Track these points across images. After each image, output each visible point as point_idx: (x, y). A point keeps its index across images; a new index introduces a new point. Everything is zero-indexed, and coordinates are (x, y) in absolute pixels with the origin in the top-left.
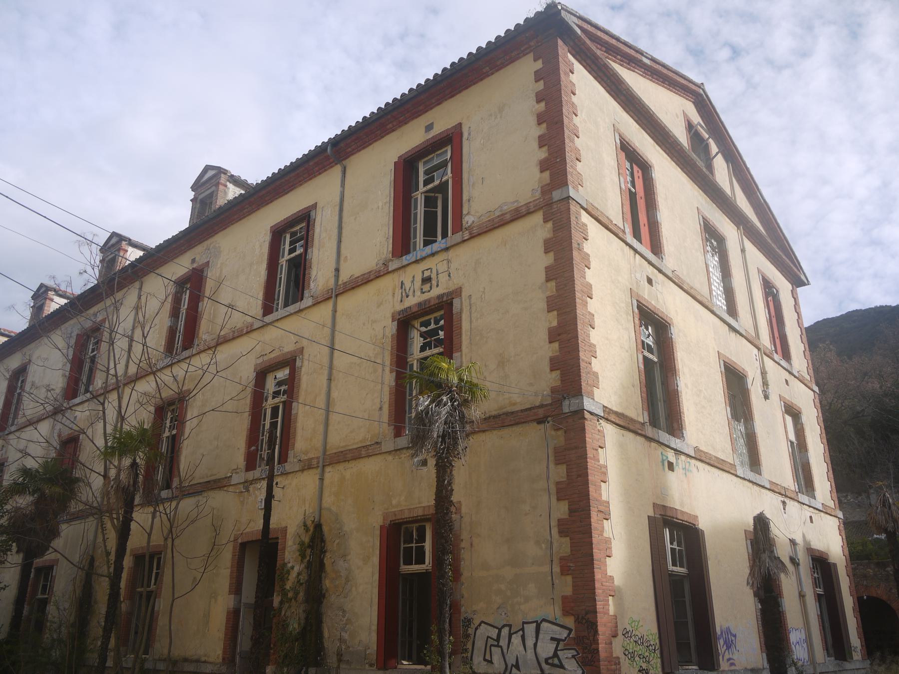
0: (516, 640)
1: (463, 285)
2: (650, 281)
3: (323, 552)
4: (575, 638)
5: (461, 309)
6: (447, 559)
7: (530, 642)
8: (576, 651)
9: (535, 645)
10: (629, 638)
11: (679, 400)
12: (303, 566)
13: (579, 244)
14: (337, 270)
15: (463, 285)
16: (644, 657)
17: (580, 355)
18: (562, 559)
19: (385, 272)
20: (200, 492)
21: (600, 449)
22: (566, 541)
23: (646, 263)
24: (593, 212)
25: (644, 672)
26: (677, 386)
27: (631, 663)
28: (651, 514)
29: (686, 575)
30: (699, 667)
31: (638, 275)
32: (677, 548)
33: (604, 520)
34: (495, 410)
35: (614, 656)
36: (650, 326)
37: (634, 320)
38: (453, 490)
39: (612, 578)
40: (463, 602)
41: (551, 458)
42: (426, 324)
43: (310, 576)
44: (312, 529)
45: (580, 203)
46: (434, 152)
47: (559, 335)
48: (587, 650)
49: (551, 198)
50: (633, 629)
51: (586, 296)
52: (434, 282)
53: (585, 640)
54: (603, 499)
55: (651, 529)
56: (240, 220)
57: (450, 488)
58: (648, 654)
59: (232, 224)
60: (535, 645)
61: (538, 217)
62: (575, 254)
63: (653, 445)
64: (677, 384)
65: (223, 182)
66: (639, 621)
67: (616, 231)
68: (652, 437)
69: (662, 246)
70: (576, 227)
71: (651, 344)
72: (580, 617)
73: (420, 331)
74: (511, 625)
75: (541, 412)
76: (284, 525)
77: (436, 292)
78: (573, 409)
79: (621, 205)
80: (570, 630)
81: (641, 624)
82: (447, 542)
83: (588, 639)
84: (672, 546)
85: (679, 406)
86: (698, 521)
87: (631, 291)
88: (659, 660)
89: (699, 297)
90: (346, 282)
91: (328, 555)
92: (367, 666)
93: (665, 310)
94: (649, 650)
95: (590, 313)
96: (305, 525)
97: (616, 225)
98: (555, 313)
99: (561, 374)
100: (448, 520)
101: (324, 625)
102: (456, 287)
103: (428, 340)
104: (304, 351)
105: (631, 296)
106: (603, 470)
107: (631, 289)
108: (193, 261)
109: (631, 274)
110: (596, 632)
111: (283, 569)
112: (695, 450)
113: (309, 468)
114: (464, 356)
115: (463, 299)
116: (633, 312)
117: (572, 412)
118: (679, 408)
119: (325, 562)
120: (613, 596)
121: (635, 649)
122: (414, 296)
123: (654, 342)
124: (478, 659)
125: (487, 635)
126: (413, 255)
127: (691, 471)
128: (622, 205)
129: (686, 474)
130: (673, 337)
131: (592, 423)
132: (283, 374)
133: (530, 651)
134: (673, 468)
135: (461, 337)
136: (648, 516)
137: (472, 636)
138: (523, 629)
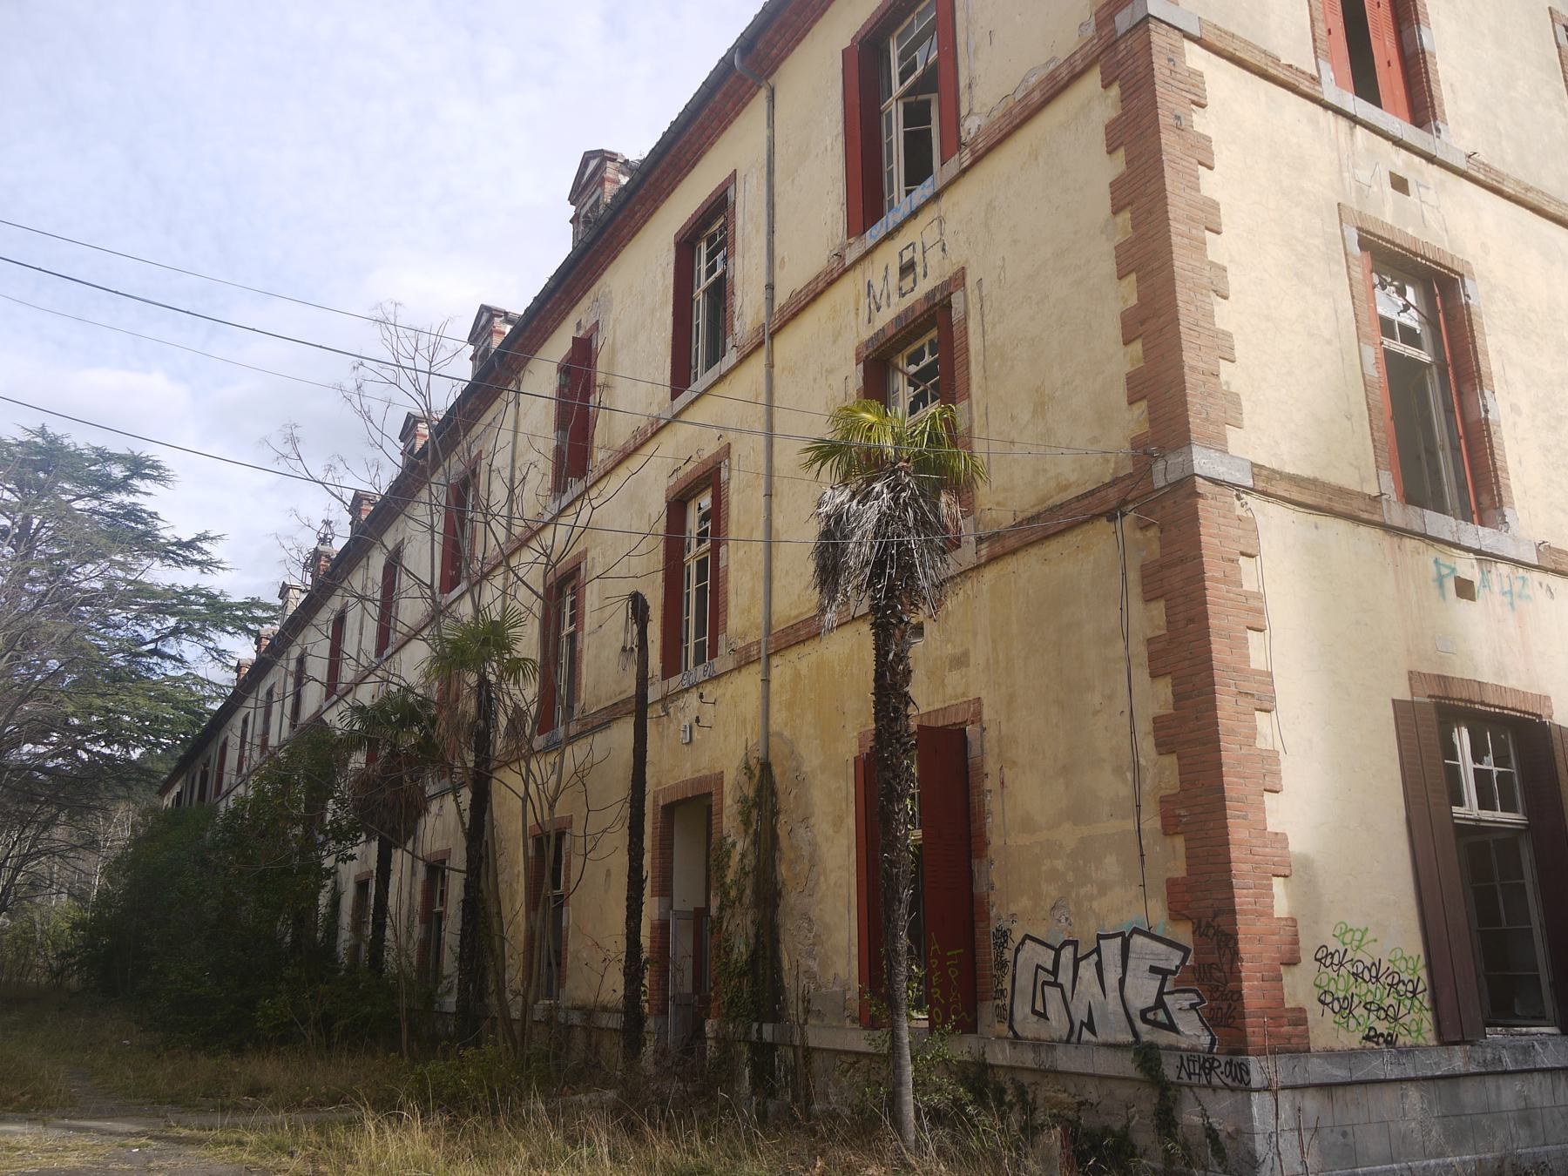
0: (1087, 971)
1: (967, 261)
2: (1400, 184)
3: (775, 813)
4: (1194, 968)
5: (966, 313)
6: (900, 810)
7: (1112, 977)
8: (1199, 995)
9: (1122, 982)
10: (1335, 968)
11: (1490, 441)
12: (748, 840)
13: (1178, 118)
14: (770, 287)
15: (967, 261)
16: (1380, 1008)
17: (1184, 359)
18: (1164, 801)
19: (840, 270)
20: (605, 724)
21: (1242, 560)
22: (1171, 761)
23: (1388, 144)
24: (1218, 44)
25: (1381, 1040)
26: (1487, 411)
27: (1342, 1020)
28: (1403, 693)
29: (1523, 827)
30: (1561, 1029)
31: (1364, 175)
32: (1495, 770)
33: (1257, 712)
34: (1032, 507)
35: (1287, 1006)
36: (1412, 285)
37: (1349, 273)
38: (910, 672)
39: (1281, 839)
40: (992, 898)
41: (1135, 589)
42: (915, 358)
43: (758, 858)
44: (757, 772)
45: (1181, 27)
46: (911, 11)
47: (1142, 323)
48: (1219, 993)
49: (1115, 31)
50: (1348, 947)
51: (1203, 227)
52: (919, 270)
53: (1213, 971)
54: (1253, 666)
55: (1399, 722)
56: (633, 235)
57: (901, 667)
58: (1394, 1002)
59: (624, 246)
60: (1122, 982)
61: (1092, 82)
62: (1168, 139)
63: (1409, 543)
64: (1485, 406)
65: (611, 176)
66: (1367, 929)
67: (1291, 80)
68: (1403, 525)
69: (1436, 103)
70: (1171, 81)
71: (1415, 325)
72: (1203, 923)
73: (907, 374)
74: (1077, 941)
75: (1113, 495)
76: (718, 770)
77: (924, 287)
78: (1172, 478)
79: (1309, 23)
80: (1186, 951)
81: (1370, 936)
82: (897, 776)
83: (1220, 971)
84: (1478, 766)
85: (1492, 454)
86: (1550, 707)
87: (1339, 210)
88: (1429, 1015)
89: (1552, 209)
90: (783, 307)
91: (782, 818)
92: (848, 1021)
93: (1447, 245)
94: (1398, 993)
95: (1213, 264)
96: (747, 767)
97: (1290, 66)
98: (1133, 277)
99: (1149, 407)
100: (898, 732)
101: (782, 947)
102: (956, 268)
103: (922, 388)
104: (732, 450)
105: (1341, 220)
106: (1253, 603)
107: (1339, 204)
108: (579, 325)
109: (1341, 172)
110: (1235, 955)
111: (721, 849)
112: (1538, 550)
113: (748, 663)
114: (974, 407)
115: (969, 291)
116: (1346, 255)
117: (1170, 485)
118: (1493, 459)
119: (779, 831)
120: (1285, 876)
121: (1353, 990)
122: (889, 306)
123: (1423, 319)
124: (1022, 1010)
125: (1036, 961)
126: (882, 225)
127: (1528, 597)
128: (1312, 21)
129: (1512, 604)
130: (1470, 302)
131: (1218, 504)
132: (706, 501)
133: (1113, 995)
134: (1474, 594)
135: (968, 368)
136: (1394, 701)
137: (1010, 965)
138: (1098, 950)
